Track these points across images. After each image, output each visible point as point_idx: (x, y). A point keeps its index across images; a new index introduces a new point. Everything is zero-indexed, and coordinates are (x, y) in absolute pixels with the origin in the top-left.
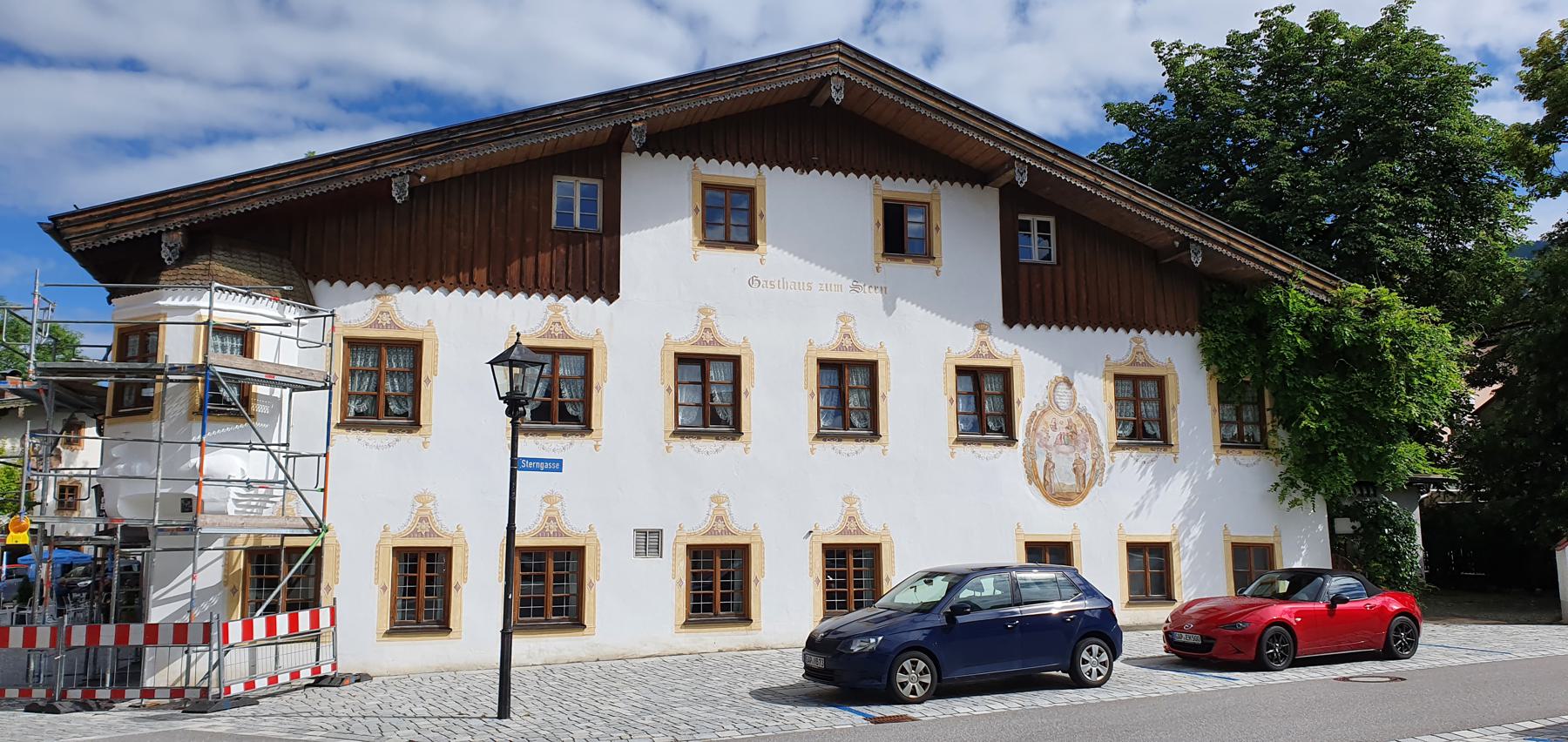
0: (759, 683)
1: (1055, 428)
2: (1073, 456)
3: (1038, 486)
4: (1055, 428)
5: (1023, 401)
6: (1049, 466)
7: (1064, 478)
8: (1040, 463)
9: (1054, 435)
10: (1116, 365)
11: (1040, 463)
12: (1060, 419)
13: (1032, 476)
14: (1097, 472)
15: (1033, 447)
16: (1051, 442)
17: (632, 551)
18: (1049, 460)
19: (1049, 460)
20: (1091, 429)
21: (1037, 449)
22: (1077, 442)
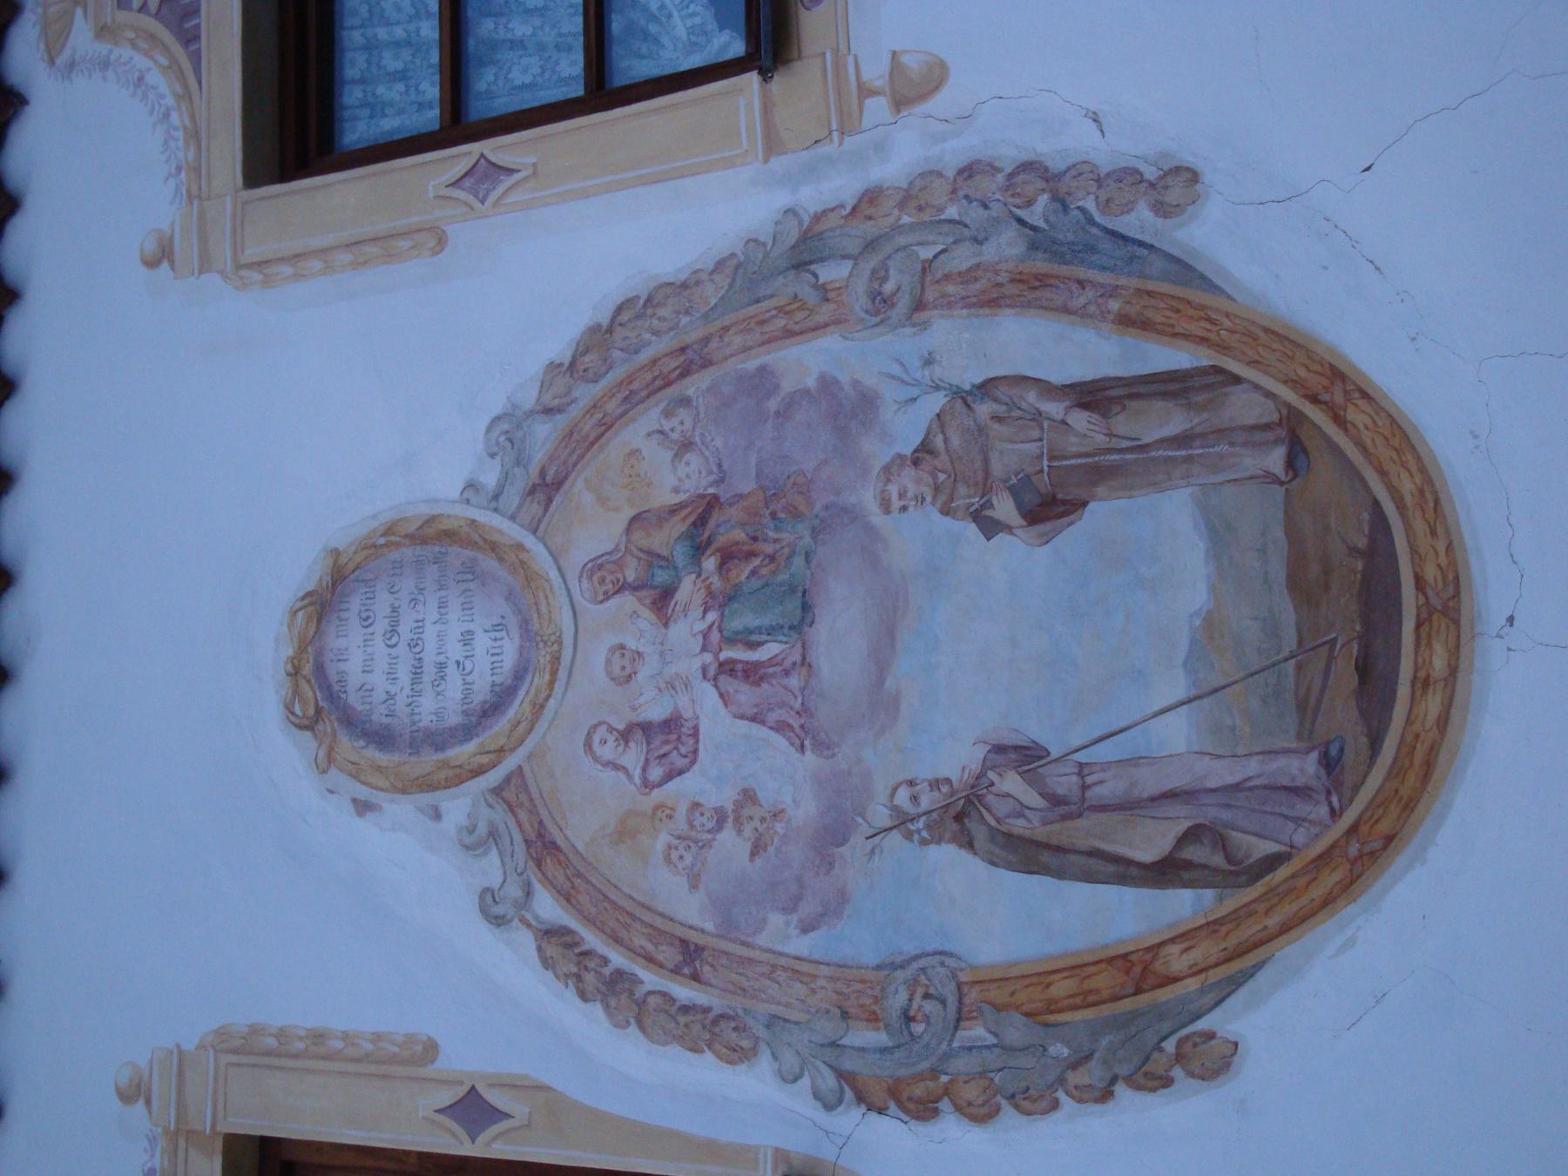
0: (747, 857)
1: (668, 739)
2: (918, 534)
3: (1238, 955)
4: (668, 739)
5: (468, 1056)
6: (1023, 814)
7: (1116, 634)
8: (1008, 919)
9: (737, 754)
10: (196, 195)
11: (1008, 919)
12: (587, 691)
13: (1131, 1027)
14: (1081, 233)
15: (856, 996)
16: (786, 778)
17: (1183, 1111)
18: (960, 816)
19: (960, 816)
20: (637, 357)
21: (857, 941)
22: (781, 499)
